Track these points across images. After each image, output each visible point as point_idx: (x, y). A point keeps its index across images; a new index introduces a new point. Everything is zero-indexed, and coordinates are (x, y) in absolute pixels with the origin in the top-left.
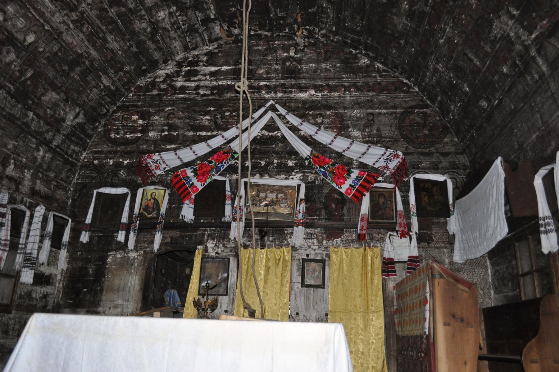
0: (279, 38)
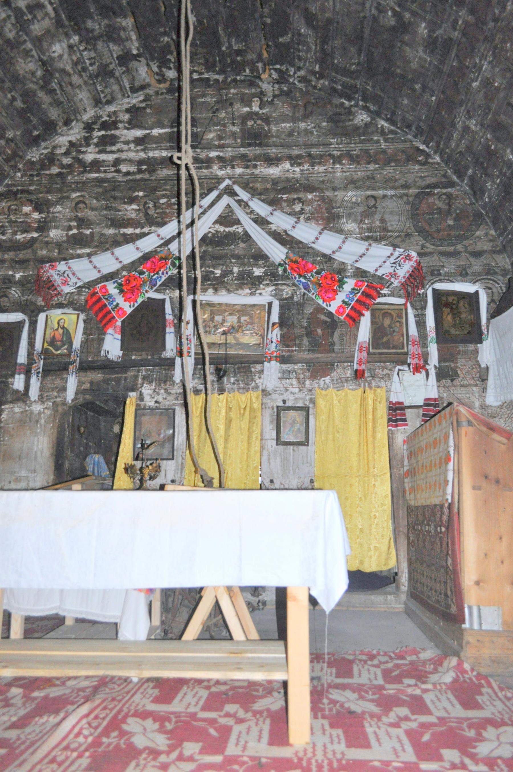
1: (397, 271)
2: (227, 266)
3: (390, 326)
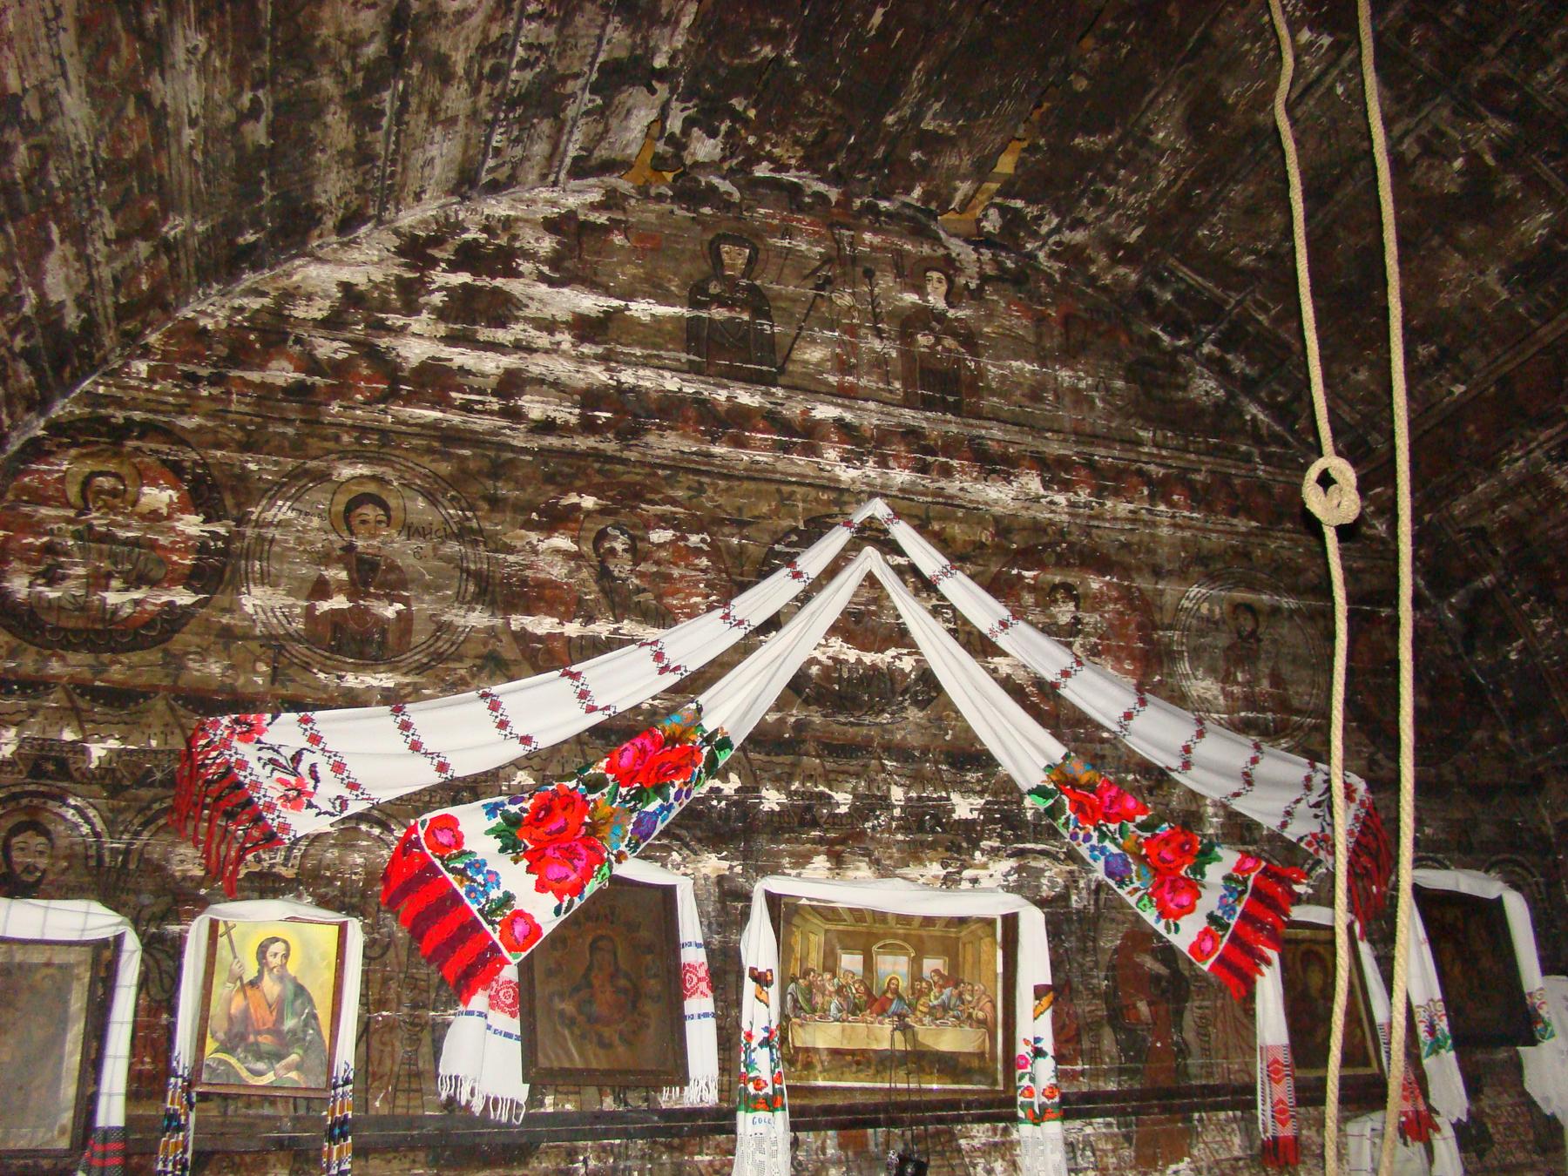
0: (878, 221)
2: (870, 782)
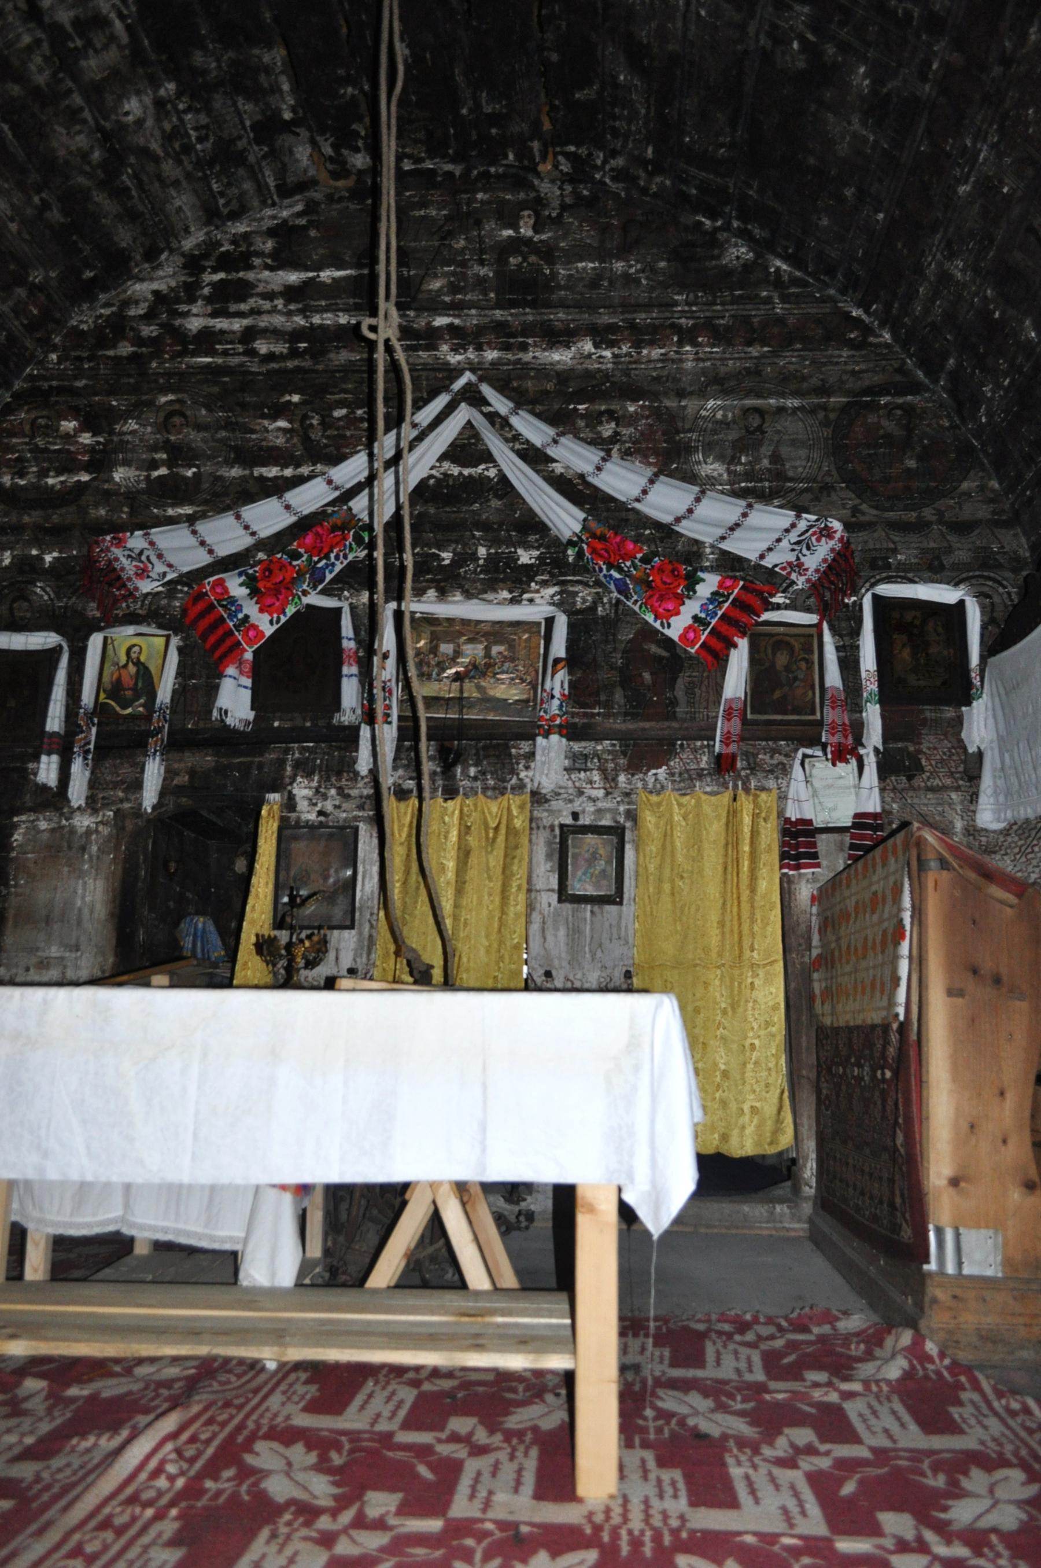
1: (803, 559)
2: (465, 545)
3: (787, 668)
